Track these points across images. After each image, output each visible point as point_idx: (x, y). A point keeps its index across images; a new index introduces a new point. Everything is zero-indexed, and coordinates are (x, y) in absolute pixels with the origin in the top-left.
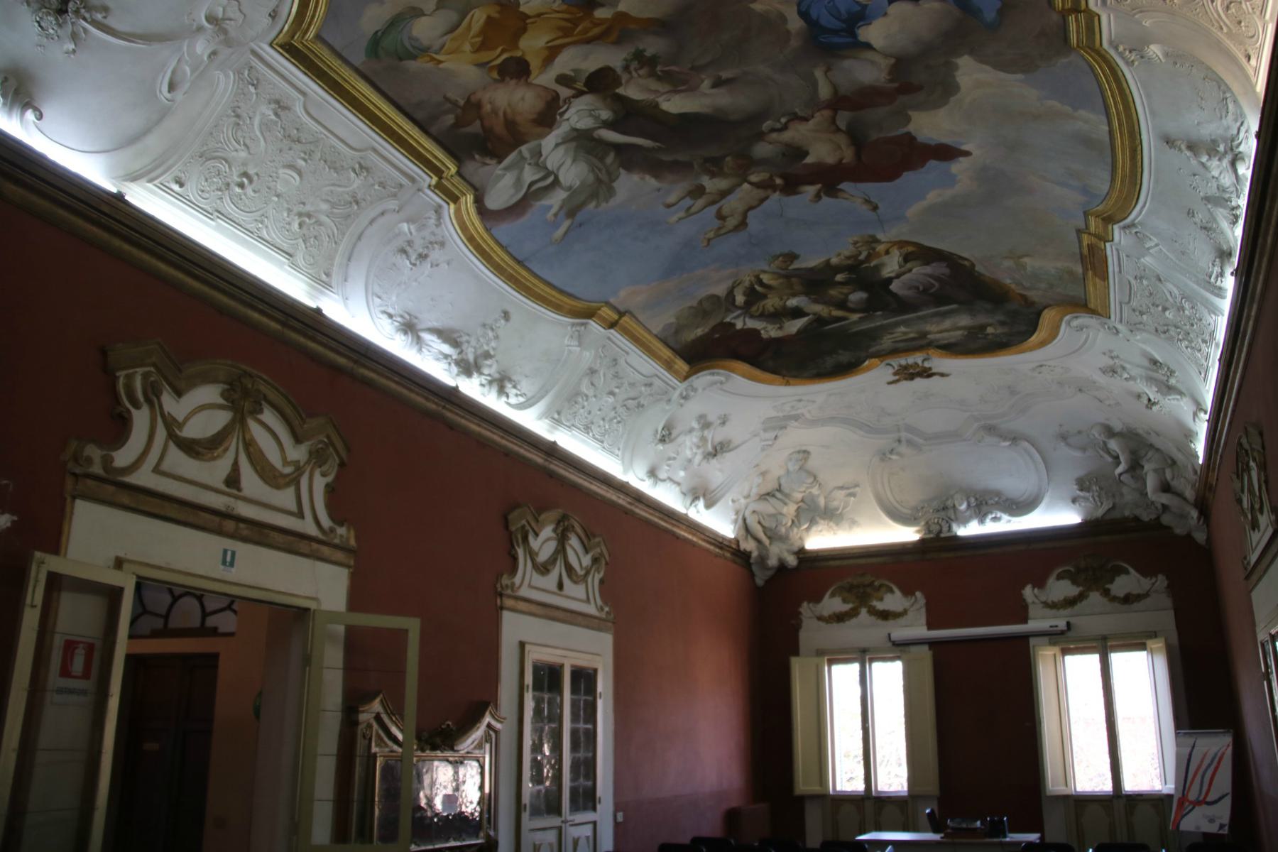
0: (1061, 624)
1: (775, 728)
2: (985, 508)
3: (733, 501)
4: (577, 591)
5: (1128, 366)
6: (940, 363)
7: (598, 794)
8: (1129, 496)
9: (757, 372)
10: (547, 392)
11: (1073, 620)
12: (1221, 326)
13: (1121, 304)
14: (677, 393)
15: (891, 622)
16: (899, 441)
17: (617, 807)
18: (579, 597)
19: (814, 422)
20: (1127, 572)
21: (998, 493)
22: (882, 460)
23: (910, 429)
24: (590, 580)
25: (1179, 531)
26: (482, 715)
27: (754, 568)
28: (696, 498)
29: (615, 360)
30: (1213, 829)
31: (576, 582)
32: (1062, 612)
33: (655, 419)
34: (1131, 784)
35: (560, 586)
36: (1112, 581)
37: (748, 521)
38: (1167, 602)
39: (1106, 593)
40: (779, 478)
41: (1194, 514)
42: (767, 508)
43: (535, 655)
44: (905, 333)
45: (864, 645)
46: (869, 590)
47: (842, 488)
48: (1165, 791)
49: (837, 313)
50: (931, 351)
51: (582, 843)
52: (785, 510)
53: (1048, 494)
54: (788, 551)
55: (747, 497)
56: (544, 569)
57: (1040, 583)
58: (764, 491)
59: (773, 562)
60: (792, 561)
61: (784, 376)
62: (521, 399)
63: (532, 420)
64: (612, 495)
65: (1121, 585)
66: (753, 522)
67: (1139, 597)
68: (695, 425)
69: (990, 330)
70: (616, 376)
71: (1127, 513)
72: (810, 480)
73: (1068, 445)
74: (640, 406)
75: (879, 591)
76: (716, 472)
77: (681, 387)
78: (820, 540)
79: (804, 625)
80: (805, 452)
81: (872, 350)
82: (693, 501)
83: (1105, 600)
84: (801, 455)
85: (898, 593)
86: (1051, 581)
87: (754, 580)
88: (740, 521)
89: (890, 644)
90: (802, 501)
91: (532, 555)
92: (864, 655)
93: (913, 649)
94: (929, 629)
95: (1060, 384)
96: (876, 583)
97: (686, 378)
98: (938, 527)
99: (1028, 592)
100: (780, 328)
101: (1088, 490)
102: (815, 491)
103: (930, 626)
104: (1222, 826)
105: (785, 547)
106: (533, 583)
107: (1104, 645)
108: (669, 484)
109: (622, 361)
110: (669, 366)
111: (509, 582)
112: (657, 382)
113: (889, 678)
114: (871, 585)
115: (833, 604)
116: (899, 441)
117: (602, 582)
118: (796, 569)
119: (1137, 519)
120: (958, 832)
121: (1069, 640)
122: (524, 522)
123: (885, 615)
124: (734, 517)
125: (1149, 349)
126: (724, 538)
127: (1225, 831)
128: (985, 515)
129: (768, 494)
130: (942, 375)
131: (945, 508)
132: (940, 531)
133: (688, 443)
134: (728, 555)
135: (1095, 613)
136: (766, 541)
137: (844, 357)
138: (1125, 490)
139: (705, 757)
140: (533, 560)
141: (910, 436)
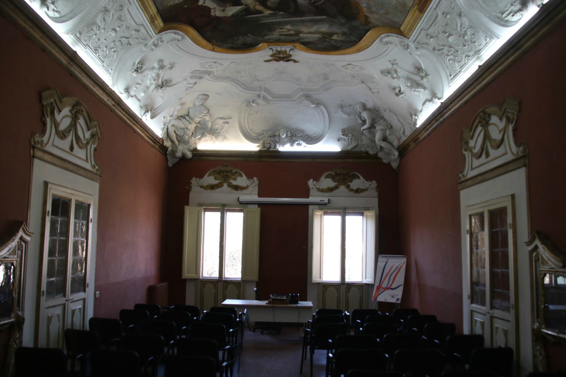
0: (326, 200)
1: (174, 243)
2: (294, 138)
3: (164, 117)
4: (81, 153)
5: (399, 70)
6: (300, 54)
7: (87, 281)
8: (365, 141)
9: (200, 38)
10: (75, 15)
11: (331, 198)
12: (491, 49)
13: (422, 30)
14: (152, 41)
15: (240, 192)
16: (258, 95)
18: (81, 157)
19: (218, 78)
20: (359, 178)
21: (302, 131)
22: (247, 106)
23: (267, 90)
24: (89, 147)
25: (385, 161)
26: (18, 231)
27: (168, 157)
28: (147, 111)
29: (122, 6)
30: (393, 301)
31: (81, 148)
32: (326, 194)
35: (72, 148)
36: (351, 182)
37: (169, 130)
38: (376, 194)
39: (348, 187)
40: (189, 109)
41: (396, 153)
43: (54, 191)
44: (289, 30)
45: (225, 202)
46: (229, 174)
47: (222, 118)
48: (365, 281)
49: (259, 8)
50: (297, 44)
51: (77, 313)
52: (189, 127)
53: (327, 135)
54: (188, 149)
55: (171, 116)
56: (62, 135)
57: (317, 179)
58: (180, 115)
59: (179, 154)
60: (189, 155)
61: (213, 44)
62: (57, 15)
63: (61, 30)
64: (105, 98)
66: (171, 130)
67: (363, 190)
68: (156, 66)
69: (335, 37)
70: (120, 18)
71: (363, 149)
72: (206, 112)
73: (343, 111)
75: (235, 175)
76: (160, 98)
77: (155, 37)
78: (205, 145)
79: (192, 189)
80: (207, 95)
81: (266, 37)
82: (145, 112)
83: (346, 190)
84: (204, 97)
86: (323, 178)
87: (167, 164)
88: (165, 129)
89: (238, 203)
90: (199, 123)
91: (56, 125)
92: (223, 208)
93: (250, 206)
94: (259, 197)
95: (354, 77)
97: (160, 32)
98: (269, 145)
99: (311, 183)
100: (223, 10)
101: (347, 135)
102: (207, 118)
103: (260, 195)
104: (398, 299)
105: (186, 147)
106: (55, 143)
107: (343, 211)
108: (134, 99)
109: (125, 9)
110: (152, 20)
111: (39, 140)
112: (142, 30)
113: (236, 221)
114: (231, 171)
115: (209, 180)
116: (259, 96)
117: (95, 150)
119: (367, 153)
120: (274, 301)
121: (328, 208)
122: (52, 100)
123: (237, 188)
124: (163, 126)
125: (420, 61)
126: (157, 137)
127: (399, 302)
128: (294, 142)
129: (182, 117)
130: (295, 61)
131: (274, 136)
132: (270, 148)
133: (149, 76)
134: (157, 147)
135: (342, 196)
136: (177, 143)
137: (250, 39)
138: (364, 138)
140: (56, 128)
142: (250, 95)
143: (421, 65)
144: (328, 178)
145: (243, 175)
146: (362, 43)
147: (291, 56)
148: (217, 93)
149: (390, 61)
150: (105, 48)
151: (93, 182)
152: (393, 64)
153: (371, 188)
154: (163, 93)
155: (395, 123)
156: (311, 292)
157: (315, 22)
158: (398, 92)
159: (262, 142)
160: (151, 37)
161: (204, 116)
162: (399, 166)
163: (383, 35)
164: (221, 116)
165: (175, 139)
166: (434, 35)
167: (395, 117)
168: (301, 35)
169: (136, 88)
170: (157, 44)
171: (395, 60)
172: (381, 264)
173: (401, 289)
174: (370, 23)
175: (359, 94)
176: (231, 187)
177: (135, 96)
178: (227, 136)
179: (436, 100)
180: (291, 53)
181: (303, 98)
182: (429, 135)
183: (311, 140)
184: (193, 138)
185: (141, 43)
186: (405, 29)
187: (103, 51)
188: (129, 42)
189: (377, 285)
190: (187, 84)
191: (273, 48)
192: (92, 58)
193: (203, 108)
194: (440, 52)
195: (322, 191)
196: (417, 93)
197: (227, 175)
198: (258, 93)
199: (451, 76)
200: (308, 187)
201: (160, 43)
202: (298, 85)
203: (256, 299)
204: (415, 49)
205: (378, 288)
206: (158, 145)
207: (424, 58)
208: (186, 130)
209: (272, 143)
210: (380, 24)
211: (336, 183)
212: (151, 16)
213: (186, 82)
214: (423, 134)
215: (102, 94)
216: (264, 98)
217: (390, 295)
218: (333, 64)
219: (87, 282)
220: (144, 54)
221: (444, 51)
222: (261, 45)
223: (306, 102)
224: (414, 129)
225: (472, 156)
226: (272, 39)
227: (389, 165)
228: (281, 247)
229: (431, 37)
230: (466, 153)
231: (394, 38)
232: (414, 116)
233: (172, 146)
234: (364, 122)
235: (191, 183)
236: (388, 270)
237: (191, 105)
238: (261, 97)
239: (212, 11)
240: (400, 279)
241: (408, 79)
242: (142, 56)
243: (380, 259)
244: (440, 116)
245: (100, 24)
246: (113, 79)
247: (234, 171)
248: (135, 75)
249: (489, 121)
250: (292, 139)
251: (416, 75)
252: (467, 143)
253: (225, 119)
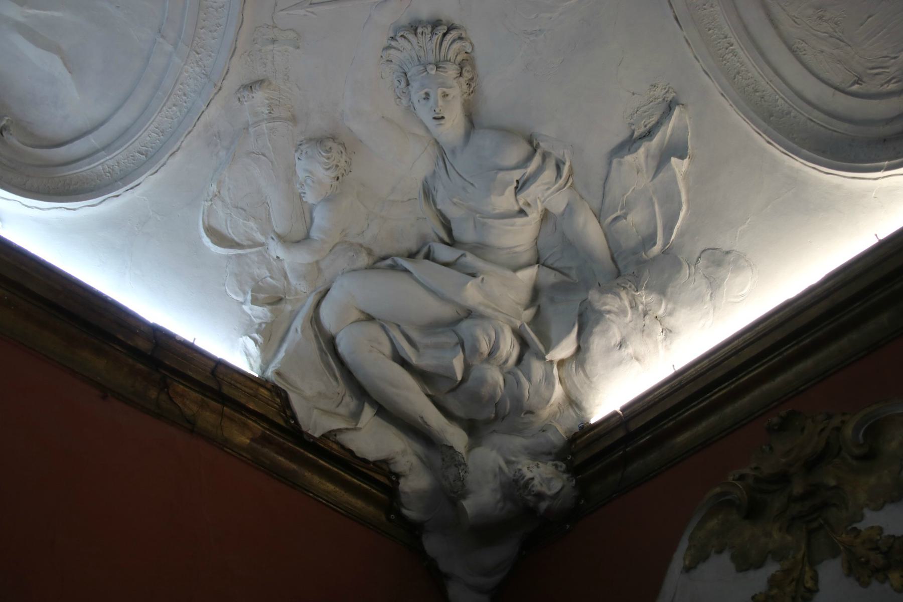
27: (432, 545)
40: (428, 193)
47: (630, 144)
54: (536, 455)
59: (481, 499)
60: (546, 478)
66: (368, 352)
72: (515, 152)
78: (628, 370)
84: (427, 43)
105: (518, 442)
136: (456, 437)
161: (520, 187)
164: (622, 135)
178: (724, 242)
253: (649, 134)
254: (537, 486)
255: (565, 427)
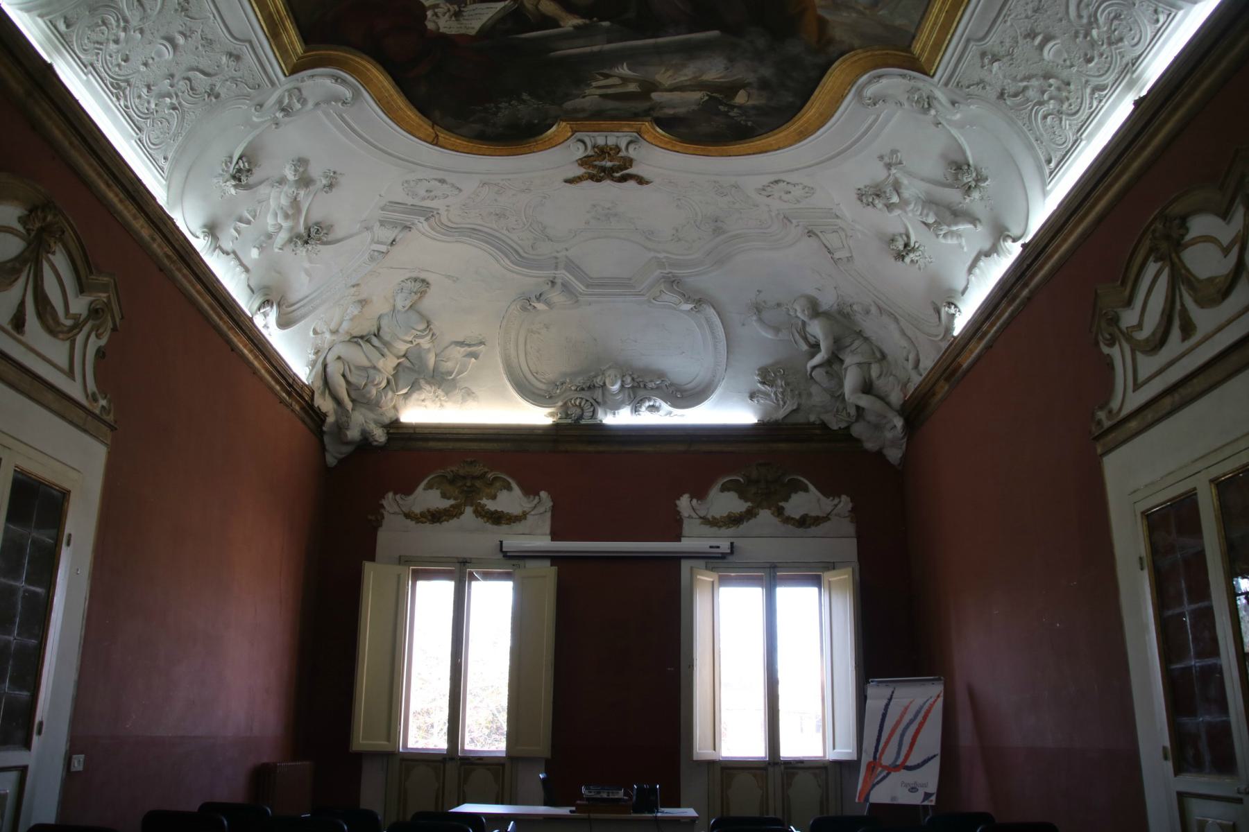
0: (724, 546)
1: (334, 654)
2: (642, 393)
3: (315, 332)
4: (57, 350)
5: (905, 181)
8: (818, 397)
9: (400, 101)
11: (737, 542)
13: (968, 41)
15: (504, 527)
16: (552, 278)
17: (75, 745)
20: (806, 490)
21: (661, 375)
22: (524, 309)
23: (572, 266)
24: (80, 339)
25: (870, 445)
27: (326, 439)
28: (267, 302)
30: (916, 799)
33: (229, 134)
34: (790, 749)
35: (18, 322)
36: (786, 499)
37: (329, 369)
38: (850, 529)
39: (779, 512)
40: (379, 318)
41: (899, 422)
42: (357, 356)
44: (625, 80)
46: (478, 484)
48: (832, 756)
52: (381, 364)
53: (723, 384)
54: (376, 422)
58: (357, 332)
59: (353, 434)
60: (380, 436)
61: (435, 123)
65: (798, 504)
66: (335, 370)
67: (817, 521)
68: (291, 176)
69: (741, 98)
71: (812, 418)
72: (423, 326)
73: (760, 320)
74: (213, 93)
76: (304, 272)
78: (422, 411)
79: (385, 522)
80: (423, 281)
81: (569, 105)
83: (776, 521)
84: (418, 285)
85: (517, 491)
86: (714, 492)
88: (319, 366)
89: (501, 556)
90: (404, 356)
92: (461, 571)
93: (531, 565)
94: (553, 540)
96: (490, 476)
97: (294, 70)
98: (579, 411)
99: (684, 503)
100: (458, 15)
102: (425, 343)
103: (555, 536)
104: (927, 796)
105: (371, 415)
107: (771, 575)
110: (274, 33)
113: (494, 601)
115: (428, 498)
116: (553, 283)
117: (101, 354)
118: (382, 448)
119: (824, 425)
121: (728, 565)
123: (497, 518)
124: (312, 357)
125: (962, 140)
127: (932, 801)
128: (642, 401)
129: (362, 337)
130: (641, 181)
132: (581, 417)
136: (349, 405)
138: (814, 389)
139: (226, 685)
141: (569, 277)
142: (530, 280)
143: (963, 153)
144: (729, 490)
145: (514, 485)
146: (811, 111)
147: (629, 162)
148: (449, 277)
149: (881, 158)
150: (145, 90)
151: (87, 438)
152: (889, 166)
153: (838, 515)
154: (310, 261)
155: (891, 339)
156: (690, 785)
157: (691, 51)
158: (901, 247)
159: (560, 404)
160: (273, 84)
161: (416, 337)
162: (904, 457)
163: (865, 78)
165: (343, 394)
166: (1002, 51)
167: (893, 326)
168: (655, 96)
169: (236, 230)
170: (289, 105)
171: (894, 152)
172: (875, 704)
173: (934, 767)
174: (830, 41)
175: (799, 270)
176: (483, 517)
177: (234, 253)
178: (474, 389)
179: (1009, 244)
180: (632, 153)
181: (662, 287)
182: (988, 347)
183: (682, 397)
184: (390, 394)
185: (247, 96)
186: (923, 50)
187: (140, 97)
188: (212, 87)
189: (867, 758)
190: (373, 241)
191: (587, 140)
192: (107, 109)
193: (414, 317)
194: (1019, 99)
195: (713, 522)
196: (951, 241)
197: (473, 486)
198: (550, 273)
199: (1049, 161)
200: (679, 513)
201: (299, 106)
202: (650, 250)
203: (545, 804)
204: (949, 105)
205: (872, 767)
206: (298, 402)
207: (972, 128)
208: (372, 372)
209: (587, 407)
210: (857, 42)
211: (749, 504)
212: (271, 15)
213: (368, 236)
214: (972, 352)
215: (135, 218)
216: (566, 287)
217: (904, 784)
218: (736, 186)
219: (38, 719)
220: (257, 132)
221: (1031, 93)
222: (554, 128)
223: (670, 297)
224: (944, 345)
225: (1133, 352)
226: (583, 110)
227: (880, 455)
228: (612, 671)
229: (995, 58)
230: (1115, 352)
231: (893, 83)
232: (944, 310)
233: (336, 412)
234: (815, 347)
235: (382, 506)
236: (896, 718)
237: (385, 308)
238: (559, 285)
239: (429, 13)
240: (931, 740)
241: (930, 202)
242: (250, 138)
243: (872, 690)
244: (1021, 282)
245: (127, 13)
246: (168, 187)
247: (490, 476)
248: (233, 191)
249: (1183, 236)
250: (637, 393)
251: (951, 186)
252: (1115, 320)
253: (469, 345)
254: (377, 438)
255: (388, 416)
